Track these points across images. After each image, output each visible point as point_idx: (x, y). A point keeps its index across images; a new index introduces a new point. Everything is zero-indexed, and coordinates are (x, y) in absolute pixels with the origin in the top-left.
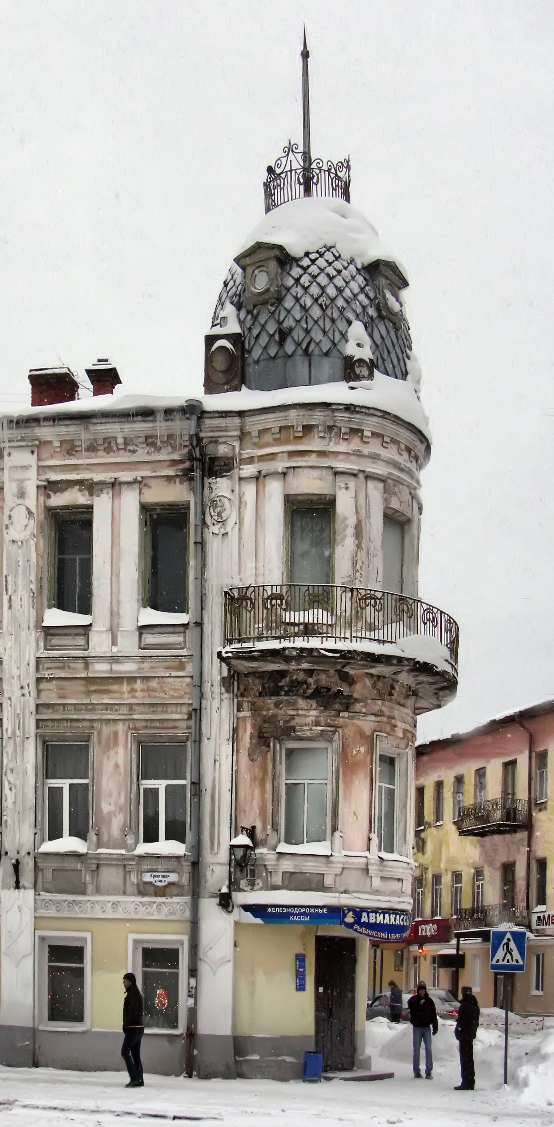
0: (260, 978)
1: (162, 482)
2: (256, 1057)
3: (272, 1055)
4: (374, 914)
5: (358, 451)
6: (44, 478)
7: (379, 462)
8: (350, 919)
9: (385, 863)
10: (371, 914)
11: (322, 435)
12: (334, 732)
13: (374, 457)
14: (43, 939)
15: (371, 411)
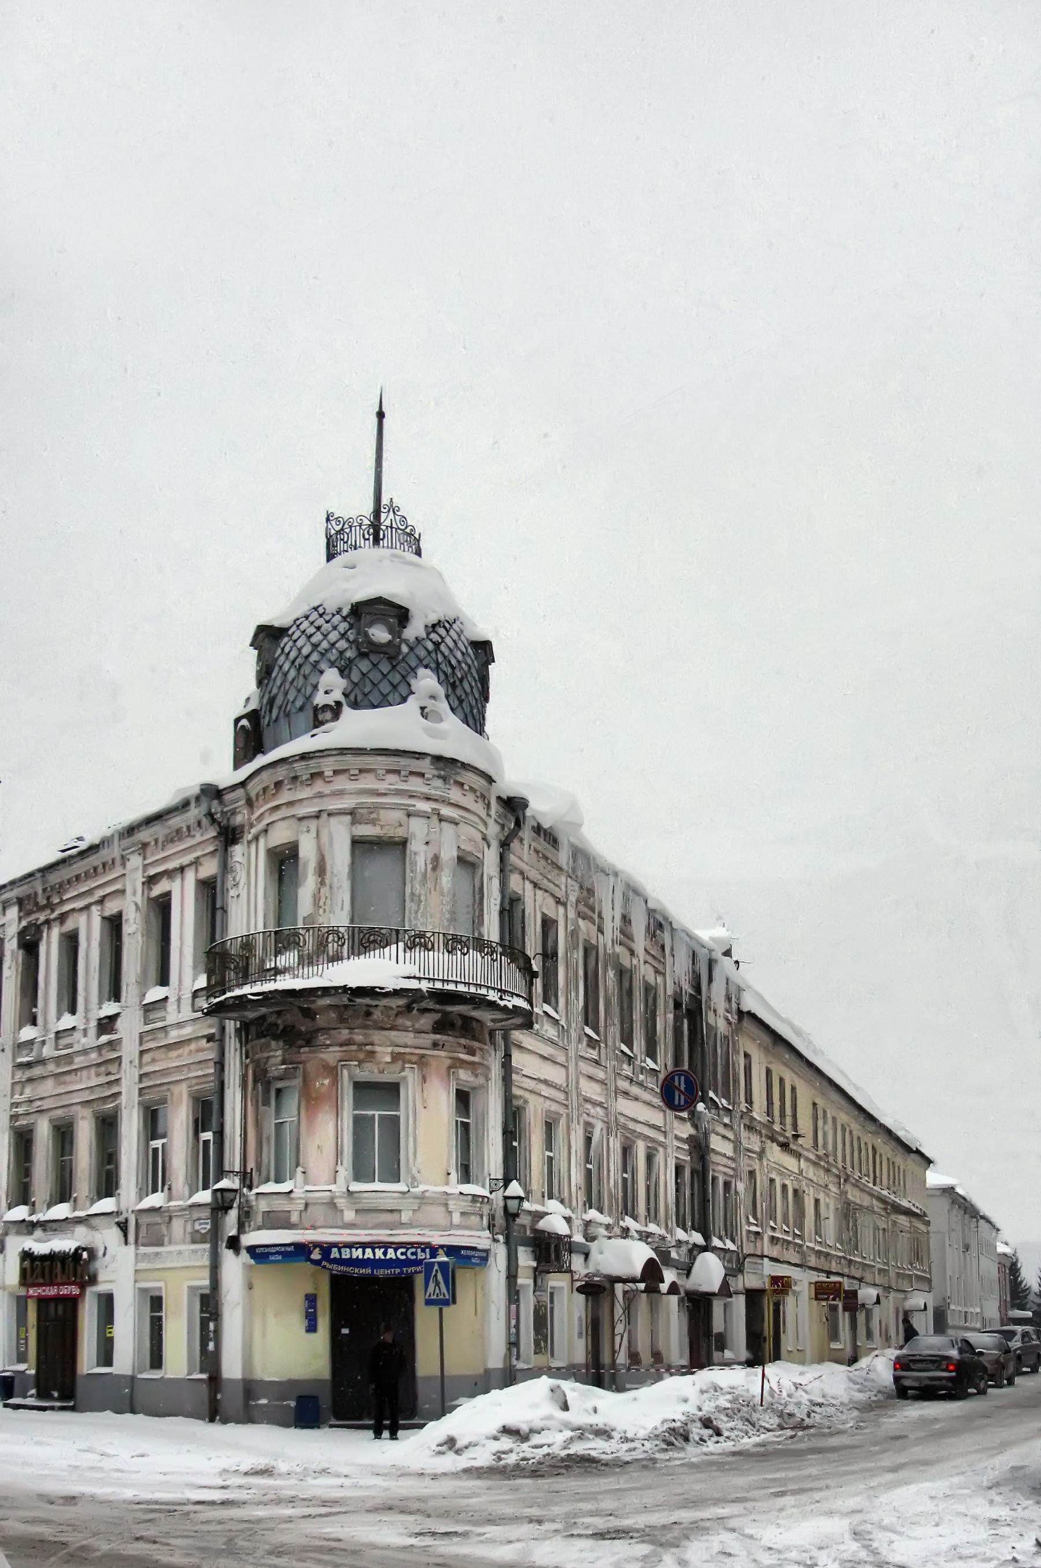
0: (271, 1319)
1: (208, 858)
2: (264, 1401)
3: (278, 1399)
4: (348, 1250)
5: (320, 792)
6: (146, 874)
7: (346, 796)
8: (316, 1255)
9: (355, 1195)
10: (343, 1250)
11: (288, 787)
12: (295, 1068)
13: (340, 793)
14: (143, 1291)
15: (325, 753)
